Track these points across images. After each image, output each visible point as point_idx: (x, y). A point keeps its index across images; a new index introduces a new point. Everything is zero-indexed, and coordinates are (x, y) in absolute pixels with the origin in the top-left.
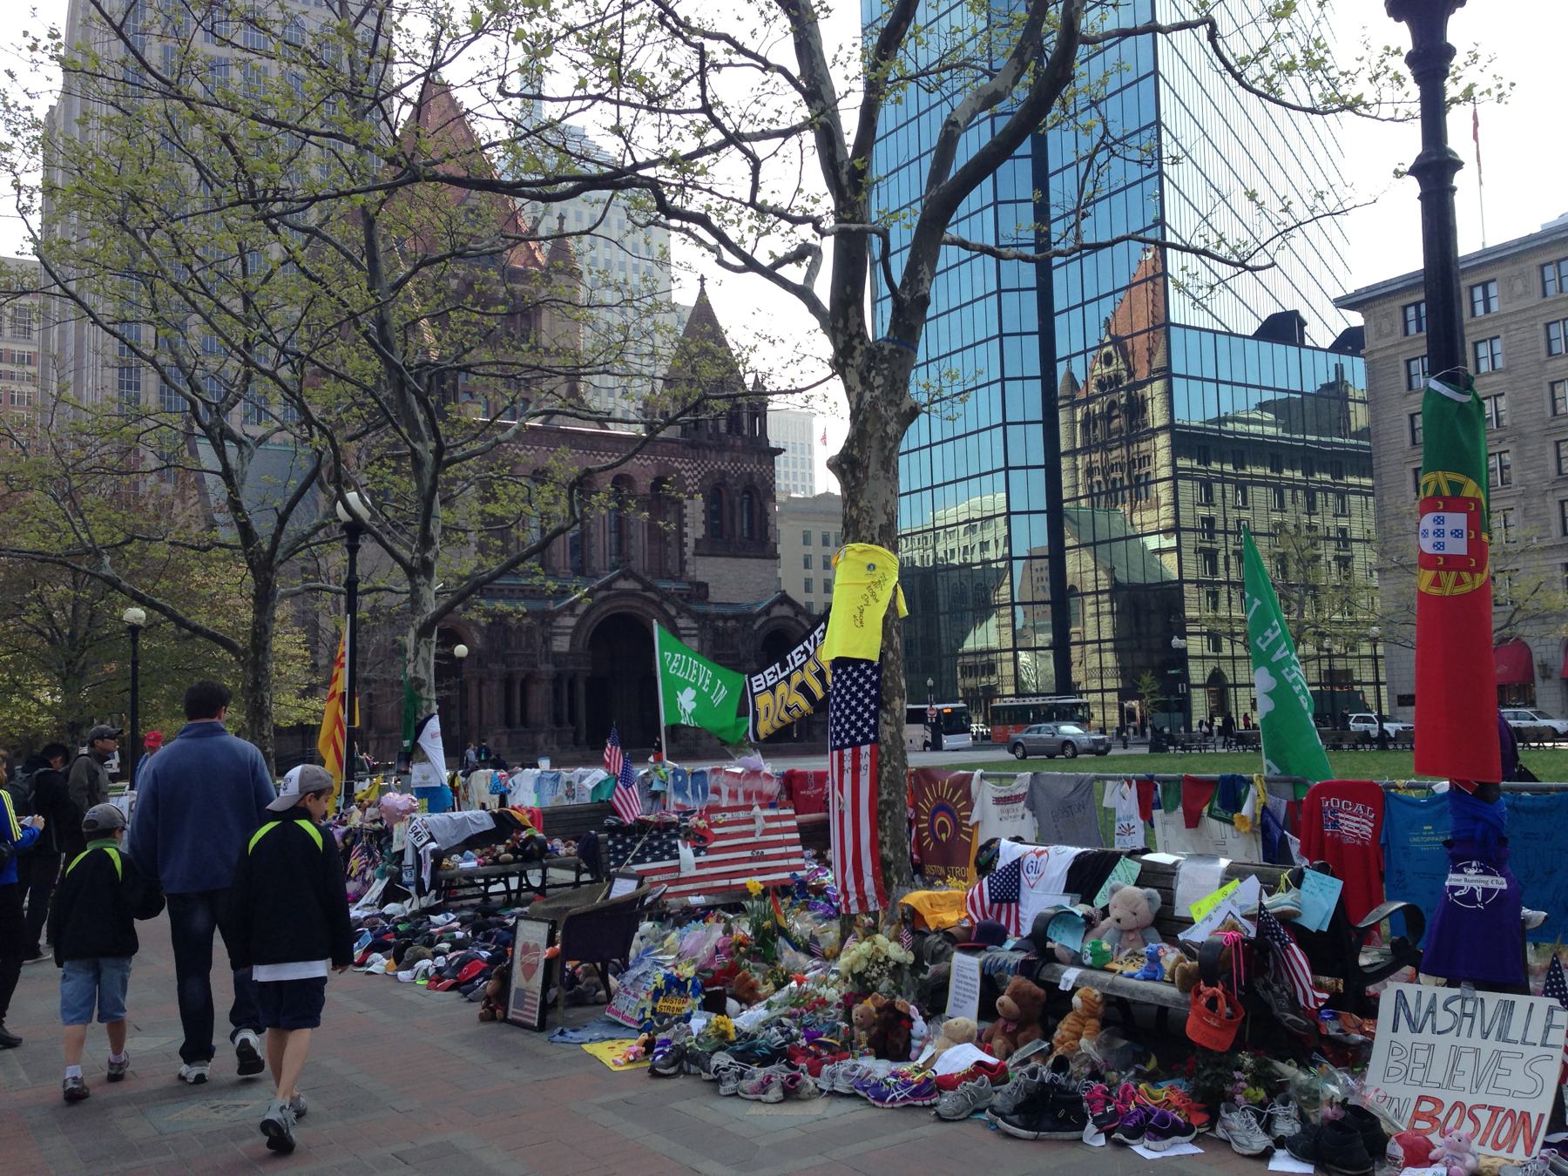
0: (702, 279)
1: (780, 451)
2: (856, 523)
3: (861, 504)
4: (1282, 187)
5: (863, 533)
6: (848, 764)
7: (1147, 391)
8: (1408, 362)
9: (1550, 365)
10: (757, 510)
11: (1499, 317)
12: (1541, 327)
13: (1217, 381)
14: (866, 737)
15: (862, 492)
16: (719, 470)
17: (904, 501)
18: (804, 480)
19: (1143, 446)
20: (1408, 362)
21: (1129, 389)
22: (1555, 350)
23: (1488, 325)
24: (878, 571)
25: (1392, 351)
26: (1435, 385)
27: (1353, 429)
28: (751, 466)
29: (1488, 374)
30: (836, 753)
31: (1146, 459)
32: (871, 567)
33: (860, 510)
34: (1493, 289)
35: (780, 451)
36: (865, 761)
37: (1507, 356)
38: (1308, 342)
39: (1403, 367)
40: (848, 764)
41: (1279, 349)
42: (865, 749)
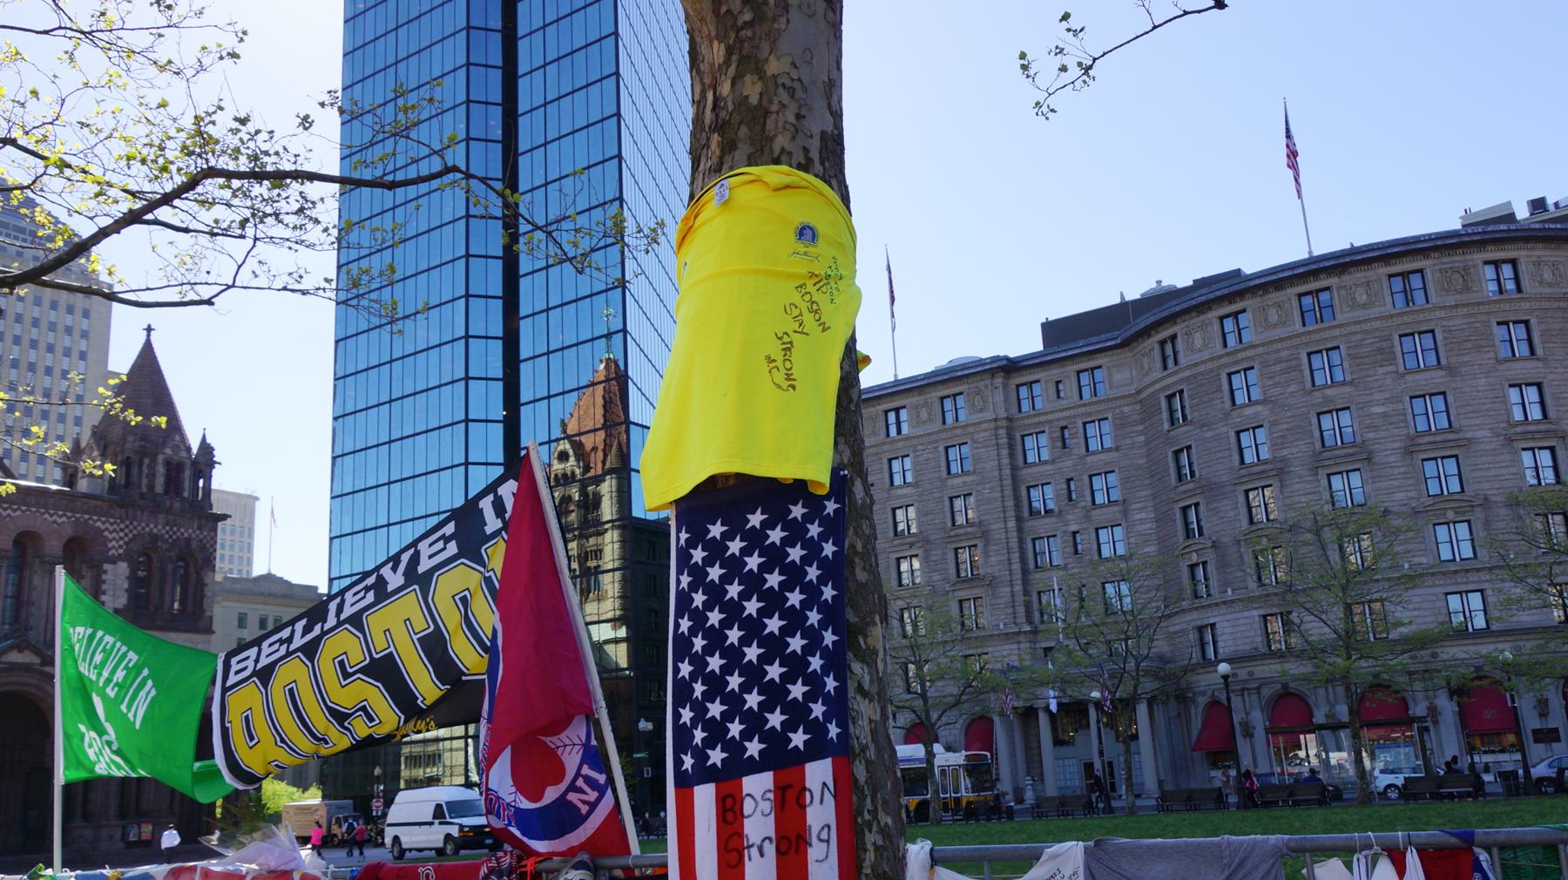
0: (149, 329)
1: (224, 517)
2: (757, 115)
3: (773, 67)
5: (781, 142)
6: (759, 825)
9: (950, 482)
10: (193, 577)
11: (908, 438)
12: (942, 449)
14: (816, 730)
15: (773, 38)
16: (151, 533)
18: (241, 563)
19: (592, 541)
22: (954, 471)
23: (900, 445)
24: (821, 248)
26: (219, 803)
28: (188, 531)
29: (900, 487)
30: (705, 796)
31: (598, 553)
32: (806, 233)
33: (771, 84)
34: (904, 414)
35: (224, 517)
36: (820, 814)
37: (915, 471)
40: (759, 825)
42: (818, 773)
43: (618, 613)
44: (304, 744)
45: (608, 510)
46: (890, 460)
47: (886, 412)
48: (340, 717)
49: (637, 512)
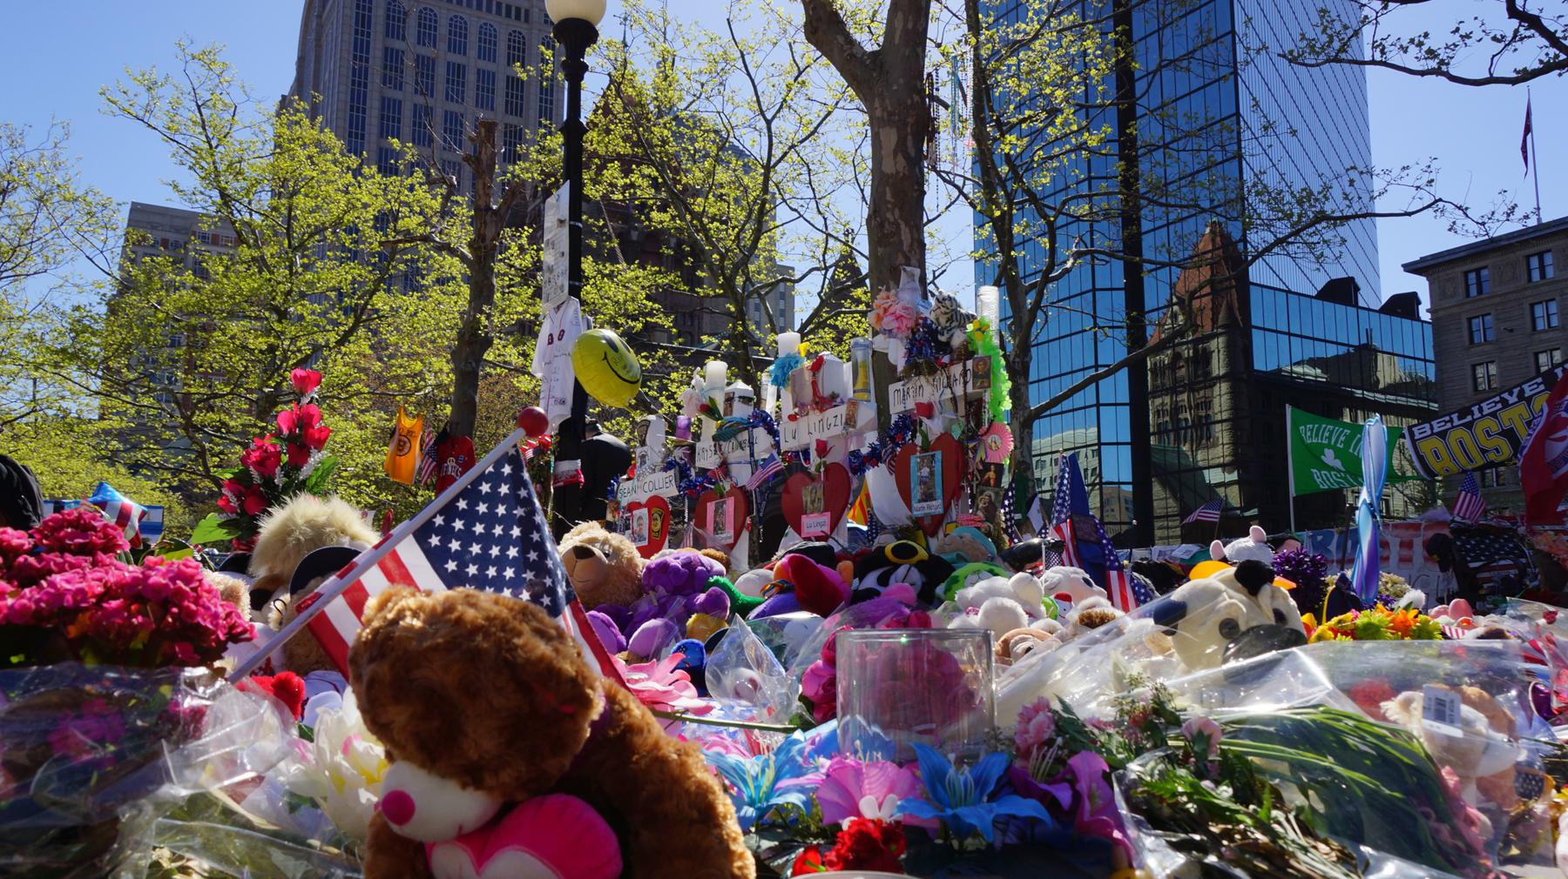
4: (1323, 168)
7: (1213, 344)
8: (1470, 320)
11: (1553, 282)
12: (1527, 306)
13: (1289, 334)
17: (1031, 387)
20: (1470, 320)
21: (1196, 342)
25: (1455, 310)
27: (1381, 386)
29: (1544, 331)
31: (1208, 404)
34: (1548, 259)
38: (1361, 303)
39: (1465, 325)
41: (1340, 308)
43: (1228, 459)
44: (1463, 460)
45: (1218, 366)
46: (1532, 306)
47: (1528, 257)
48: (1484, 451)
49: (1259, 365)
